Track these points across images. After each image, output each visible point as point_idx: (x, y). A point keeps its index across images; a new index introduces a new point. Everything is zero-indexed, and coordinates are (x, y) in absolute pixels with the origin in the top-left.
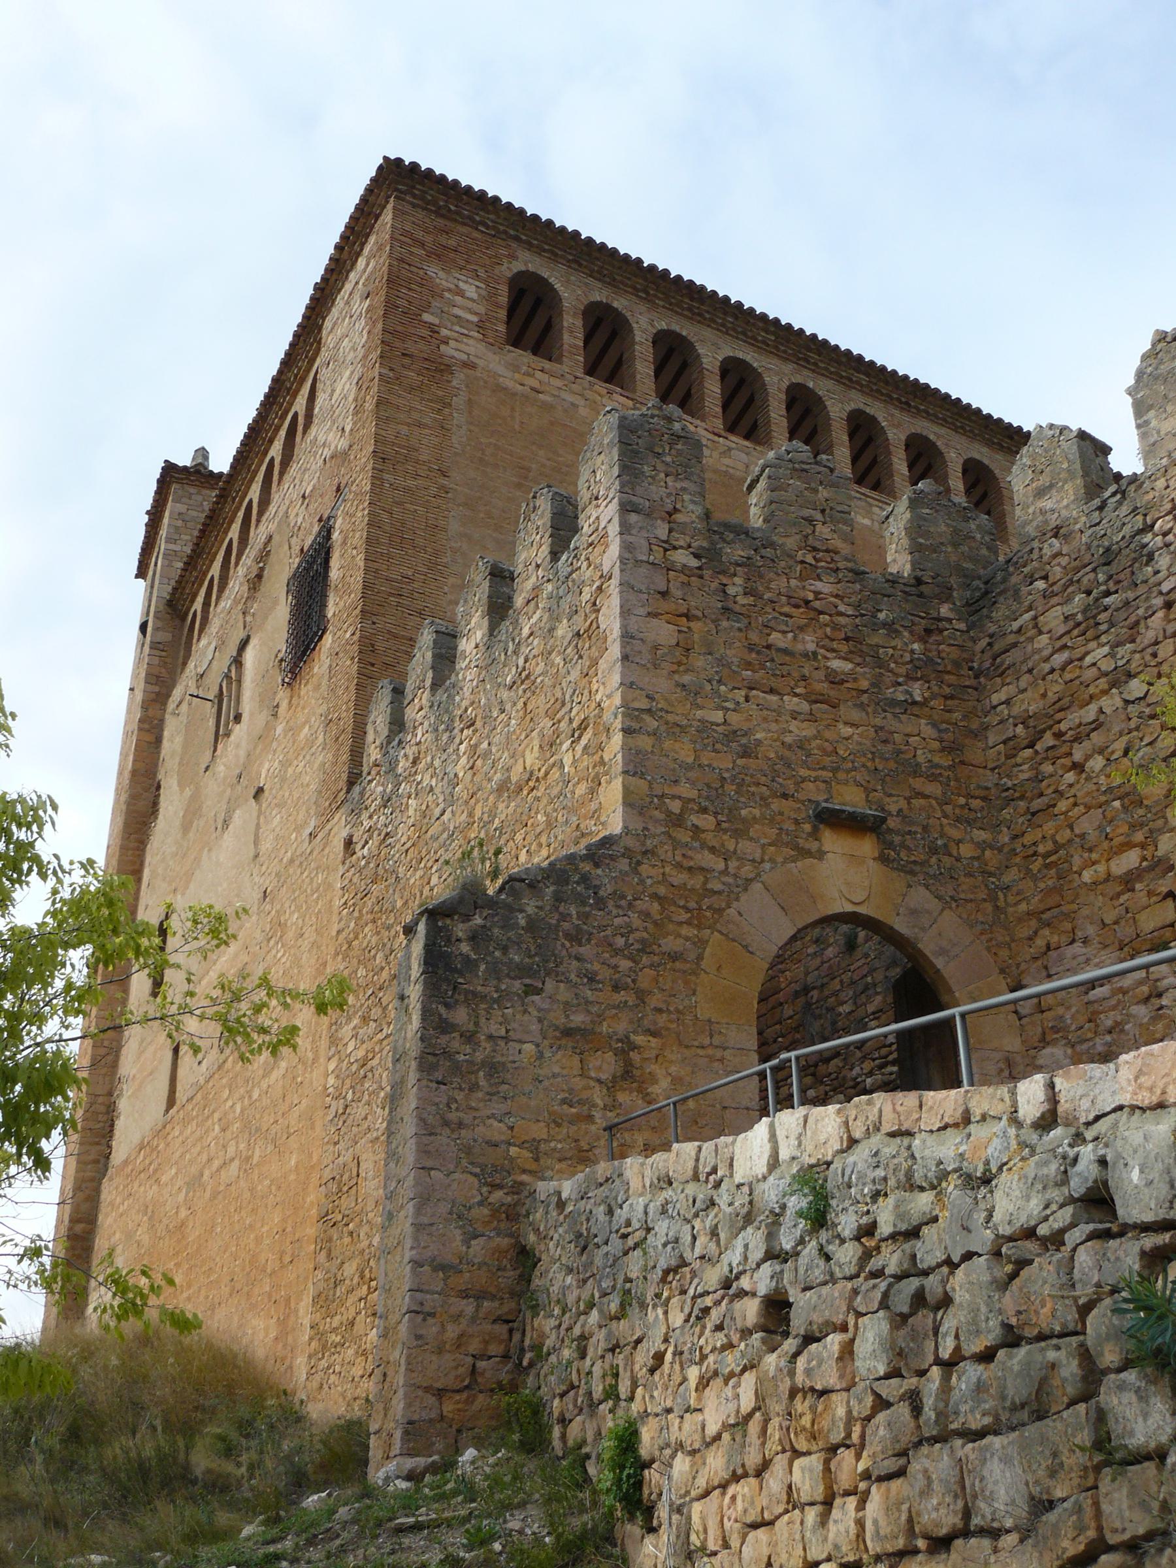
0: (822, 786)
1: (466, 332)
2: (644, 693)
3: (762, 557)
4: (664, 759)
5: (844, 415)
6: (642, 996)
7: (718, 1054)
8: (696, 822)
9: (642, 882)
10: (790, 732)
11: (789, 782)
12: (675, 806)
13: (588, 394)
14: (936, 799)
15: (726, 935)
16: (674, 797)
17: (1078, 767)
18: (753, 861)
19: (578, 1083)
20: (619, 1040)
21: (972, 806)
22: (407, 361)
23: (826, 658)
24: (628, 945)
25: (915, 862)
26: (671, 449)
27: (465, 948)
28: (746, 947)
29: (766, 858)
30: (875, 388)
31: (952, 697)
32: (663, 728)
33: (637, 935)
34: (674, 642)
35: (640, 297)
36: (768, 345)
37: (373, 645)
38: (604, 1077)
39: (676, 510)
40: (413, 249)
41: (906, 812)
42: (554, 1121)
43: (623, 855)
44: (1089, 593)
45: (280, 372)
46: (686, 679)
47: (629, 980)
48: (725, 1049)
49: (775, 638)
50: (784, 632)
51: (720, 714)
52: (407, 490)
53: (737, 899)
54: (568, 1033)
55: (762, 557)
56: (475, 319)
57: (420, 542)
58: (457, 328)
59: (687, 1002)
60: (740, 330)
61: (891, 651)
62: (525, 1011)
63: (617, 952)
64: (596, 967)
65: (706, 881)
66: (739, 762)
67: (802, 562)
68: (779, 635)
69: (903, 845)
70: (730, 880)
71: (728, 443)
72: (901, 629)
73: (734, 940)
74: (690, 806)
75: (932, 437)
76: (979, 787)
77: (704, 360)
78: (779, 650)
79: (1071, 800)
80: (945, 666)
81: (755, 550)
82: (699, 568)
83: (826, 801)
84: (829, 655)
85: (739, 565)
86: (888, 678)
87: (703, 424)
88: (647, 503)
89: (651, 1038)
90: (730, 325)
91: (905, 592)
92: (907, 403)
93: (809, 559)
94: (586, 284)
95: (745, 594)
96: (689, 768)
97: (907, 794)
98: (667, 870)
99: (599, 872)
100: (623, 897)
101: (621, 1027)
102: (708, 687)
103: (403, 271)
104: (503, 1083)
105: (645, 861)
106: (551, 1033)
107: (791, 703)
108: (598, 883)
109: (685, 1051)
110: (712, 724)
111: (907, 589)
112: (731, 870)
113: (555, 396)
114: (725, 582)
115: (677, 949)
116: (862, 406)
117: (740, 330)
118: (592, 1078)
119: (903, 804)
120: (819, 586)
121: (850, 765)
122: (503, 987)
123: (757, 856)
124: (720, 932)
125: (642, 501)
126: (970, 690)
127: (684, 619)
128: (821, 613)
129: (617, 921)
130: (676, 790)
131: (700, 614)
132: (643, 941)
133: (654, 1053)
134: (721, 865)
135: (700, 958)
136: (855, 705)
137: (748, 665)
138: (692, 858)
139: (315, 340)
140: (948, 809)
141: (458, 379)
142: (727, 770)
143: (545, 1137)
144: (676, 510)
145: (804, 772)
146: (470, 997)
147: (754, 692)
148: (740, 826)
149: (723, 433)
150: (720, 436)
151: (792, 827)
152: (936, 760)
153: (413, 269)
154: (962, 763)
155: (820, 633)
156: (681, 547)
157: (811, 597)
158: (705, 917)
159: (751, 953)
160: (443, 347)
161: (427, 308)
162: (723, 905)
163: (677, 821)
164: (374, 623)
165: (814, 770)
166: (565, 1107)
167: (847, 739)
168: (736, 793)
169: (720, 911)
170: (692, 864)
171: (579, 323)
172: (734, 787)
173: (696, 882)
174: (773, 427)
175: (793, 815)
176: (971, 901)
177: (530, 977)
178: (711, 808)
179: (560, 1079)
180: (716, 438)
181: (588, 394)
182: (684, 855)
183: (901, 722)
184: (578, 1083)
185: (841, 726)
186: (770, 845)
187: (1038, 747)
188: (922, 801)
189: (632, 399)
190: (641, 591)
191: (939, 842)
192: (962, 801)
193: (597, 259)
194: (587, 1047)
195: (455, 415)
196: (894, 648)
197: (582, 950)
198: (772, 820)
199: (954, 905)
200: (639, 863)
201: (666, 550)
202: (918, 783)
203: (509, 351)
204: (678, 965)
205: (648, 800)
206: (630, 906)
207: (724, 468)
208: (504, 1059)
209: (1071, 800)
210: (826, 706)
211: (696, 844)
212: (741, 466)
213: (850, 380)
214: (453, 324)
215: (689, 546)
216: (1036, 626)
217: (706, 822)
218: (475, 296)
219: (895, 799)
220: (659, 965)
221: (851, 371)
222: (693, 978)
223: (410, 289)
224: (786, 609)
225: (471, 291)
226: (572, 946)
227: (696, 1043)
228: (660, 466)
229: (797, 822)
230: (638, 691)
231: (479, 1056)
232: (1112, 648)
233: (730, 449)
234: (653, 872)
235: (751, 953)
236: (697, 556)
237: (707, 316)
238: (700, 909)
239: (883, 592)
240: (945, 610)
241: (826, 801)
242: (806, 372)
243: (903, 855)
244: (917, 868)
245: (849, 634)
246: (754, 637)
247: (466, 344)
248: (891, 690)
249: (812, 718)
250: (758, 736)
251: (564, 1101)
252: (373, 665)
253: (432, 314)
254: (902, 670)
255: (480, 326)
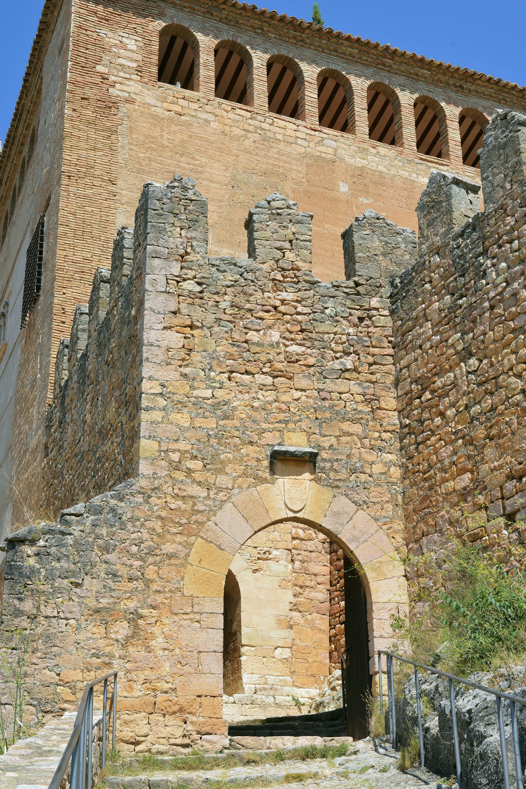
0: (277, 434)
1: (128, 76)
2: (158, 383)
3: (245, 279)
4: (170, 426)
5: (412, 102)
6: (148, 583)
7: (197, 617)
8: (188, 466)
9: (151, 509)
10: (258, 399)
11: (254, 434)
12: (175, 457)
13: (218, 112)
14: (357, 435)
15: (206, 540)
16: (174, 451)
17: (442, 414)
18: (227, 488)
19: (101, 643)
20: (132, 613)
21: (383, 438)
22: (85, 102)
23: (286, 346)
24: (139, 551)
25: (339, 480)
26: (185, 209)
27: (32, 561)
28: (219, 547)
29: (236, 486)
30: (435, 78)
31: (375, 363)
32: (170, 405)
33: (147, 543)
34: (181, 345)
35: (258, 33)
36: (354, 57)
37: (63, 309)
38: (120, 637)
39: (187, 253)
40: (89, 18)
41: (336, 446)
42: (86, 668)
43: (139, 493)
44: (453, 294)
45: (20, 98)
46: (187, 370)
47: (140, 573)
48: (201, 614)
49: (253, 336)
50: (258, 331)
51: (210, 391)
52: (86, 197)
53: (215, 515)
54: (97, 611)
55: (245, 279)
56: (134, 65)
57: (95, 233)
58: (121, 74)
59: (177, 585)
60: (332, 48)
61: (332, 336)
62: (70, 599)
63: (133, 555)
64: (118, 566)
65: (195, 504)
66: (221, 423)
67: (274, 280)
68: (254, 333)
69: (332, 469)
70: (210, 502)
71: (322, 135)
72: (341, 319)
73: (211, 542)
74: (186, 456)
75: (480, 109)
76: (389, 424)
77: (305, 75)
78: (253, 344)
79: (438, 436)
80: (371, 342)
81: (241, 275)
82: (201, 292)
83: (279, 444)
84: (288, 343)
85: (228, 287)
86: (329, 354)
87: (303, 123)
88: (167, 250)
89: (152, 610)
90: (325, 46)
91: (345, 293)
92: (461, 87)
93: (279, 277)
94: (217, 28)
95: (232, 306)
96: (187, 429)
97: (337, 434)
98: (168, 499)
99: (123, 504)
100: (138, 520)
101: (132, 605)
102: (202, 373)
103: (82, 36)
104: (54, 646)
105: (154, 495)
106: (86, 612)
107: (260, 379)
108: (121, 512)
109: (175, 617)
110: (204, 399)
111: (347, 290)
112: (212, 496)
113: (193, 116)
114: (218, 300)
115: (171, 550)
116: (426, 93)
117: (332, 48)
118: (112, 639)
119: (333, 440)
120: (284, 295)
121: (298, 418)
122: (56, 585)
123: (230, 487)
124: (202, 538)
125: (162, 249)
126: (388, 357)
127: (189, 329)
128: (284, 314)
129: (133, 536)
130: (176, 446)
131: (199, 324)
132: (149, 548)
133: (154, 620)
134: (205, 494)
135: (187, 555)
136: (304, 376)
137: (231, 357)
138: (185, 490)
139: (39, 76)
140: (366, 441)
141: (124, 108)
142: (212, 429)
143: (80, 679)
144: (187, 253)
145: (265, 426)
146: (35, 592)
147: (234, 374)
148: (219, 466)
149: (318, 128)
150: (315, 131)
151: (256, 463)
152: (360, 408)
153: (89, 33)
154: (379, 408)
155: (282, 328)
156: (189, 279)
157: (278, 303)
158: (192, 528)
159: (222, 550)
160: (111, 90)
161: (99, 61)
162: (205, 519)
163: (176, 467)
164: (64, 294)
165: (272, 423)
166: (94, 658)
167: (297, 400)
168: (218, 444)
169: (202, 524)
170: (185, 494)
171: (212, 58)
172: (216, 441)
173: (186, 506)
174: (357, 118)
175: (255, 456)
176: (378, 503)
177: (73, 577)
178: (199, 456)
179: (91, 641)
180: (313, 133)
181: (218, 112)
182: (179, 489)
183: (336, 384)
184: (101, 643)
185: (293, 391)
186: (239, 477)
187: (423, 399)
188: (348, 438)
189: (250, 112)
190: (159, 313)
191: (358, 465)
192: (376, 435)
193: (224, 9)
194: (110, 619)
195: (120, 139)
196: (335, 334)
197: (108, 556)
198: (241, 460)
199: (365, 507)
200: (150, 497)
201: (178, 282)
202: (346, 426)
203: (160, 87)
204: (173, 561)
205: (157, 454)
206: (142, 525)
207: (318, 154)
208: (55, 631)
209: (438, 436)
210: (283, 379)
211: (189, 481)
212: (330, 151)
213: (417, 75)
214: (119, 71)
215: (195, 277)
216: (425, 315)
217: (197, 465)
218: (134, 48)
219: (328, 438)
220: (160, 562)
221: (418, 69)
222: (182, 569)
223: (87, 49)
224: (260, 314)
225: (131, 44)
226: (103, 554)
227: (182, 611)
228: (177, 224)
229: (258, 460)
230: (155, 382)
231: (39, 630)
232: (462, 335)
233: (323, 139)
234: (159, 501)
235: (222, 550)
236: (199, 284)
237: (307, 41)
238: (189, 523)
239: (331, 294)
240: (374, 302)
241: (279, 444)
242: (383, 73)
243: (332, 474)
244: (340, 484)
245: (304, 327)
246: (236, 336)
247: (128, 86)
248: (331, 363)
249: (274, 388)
250: (235, 404)
251: (93, 655)
252: (64, 323)
253: (103, 65)
254: (340, 348)
255: (139, 71)
